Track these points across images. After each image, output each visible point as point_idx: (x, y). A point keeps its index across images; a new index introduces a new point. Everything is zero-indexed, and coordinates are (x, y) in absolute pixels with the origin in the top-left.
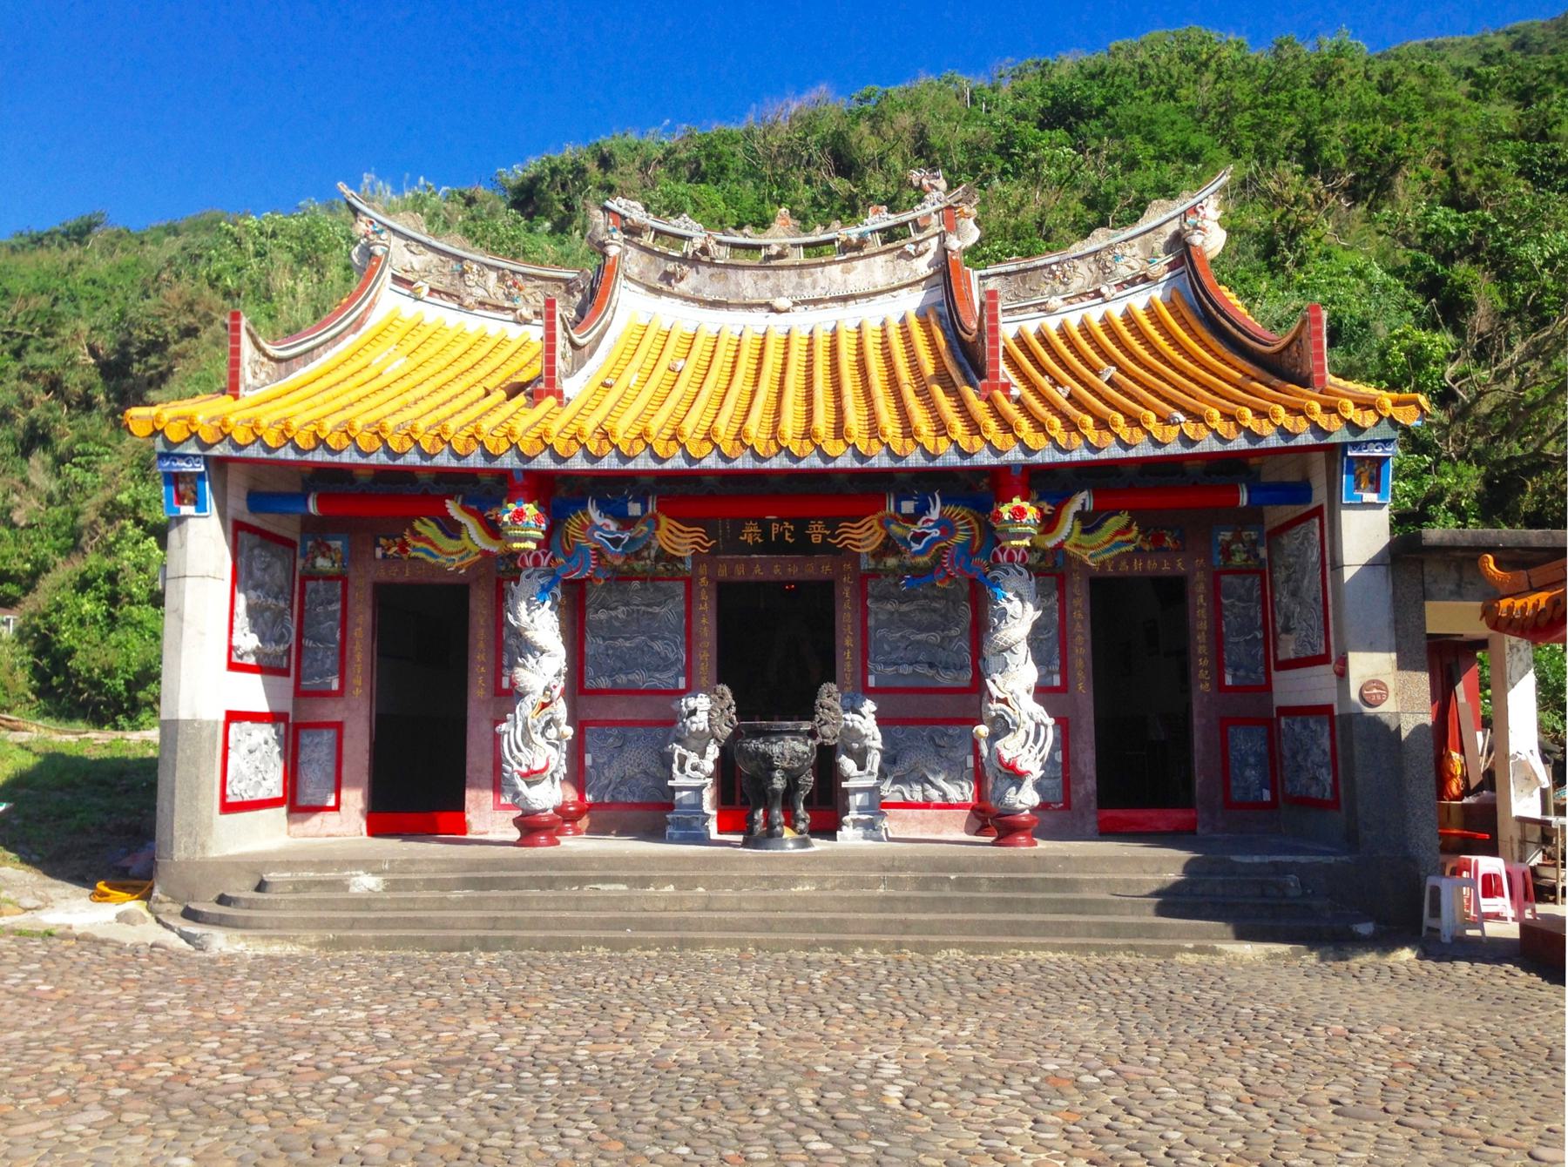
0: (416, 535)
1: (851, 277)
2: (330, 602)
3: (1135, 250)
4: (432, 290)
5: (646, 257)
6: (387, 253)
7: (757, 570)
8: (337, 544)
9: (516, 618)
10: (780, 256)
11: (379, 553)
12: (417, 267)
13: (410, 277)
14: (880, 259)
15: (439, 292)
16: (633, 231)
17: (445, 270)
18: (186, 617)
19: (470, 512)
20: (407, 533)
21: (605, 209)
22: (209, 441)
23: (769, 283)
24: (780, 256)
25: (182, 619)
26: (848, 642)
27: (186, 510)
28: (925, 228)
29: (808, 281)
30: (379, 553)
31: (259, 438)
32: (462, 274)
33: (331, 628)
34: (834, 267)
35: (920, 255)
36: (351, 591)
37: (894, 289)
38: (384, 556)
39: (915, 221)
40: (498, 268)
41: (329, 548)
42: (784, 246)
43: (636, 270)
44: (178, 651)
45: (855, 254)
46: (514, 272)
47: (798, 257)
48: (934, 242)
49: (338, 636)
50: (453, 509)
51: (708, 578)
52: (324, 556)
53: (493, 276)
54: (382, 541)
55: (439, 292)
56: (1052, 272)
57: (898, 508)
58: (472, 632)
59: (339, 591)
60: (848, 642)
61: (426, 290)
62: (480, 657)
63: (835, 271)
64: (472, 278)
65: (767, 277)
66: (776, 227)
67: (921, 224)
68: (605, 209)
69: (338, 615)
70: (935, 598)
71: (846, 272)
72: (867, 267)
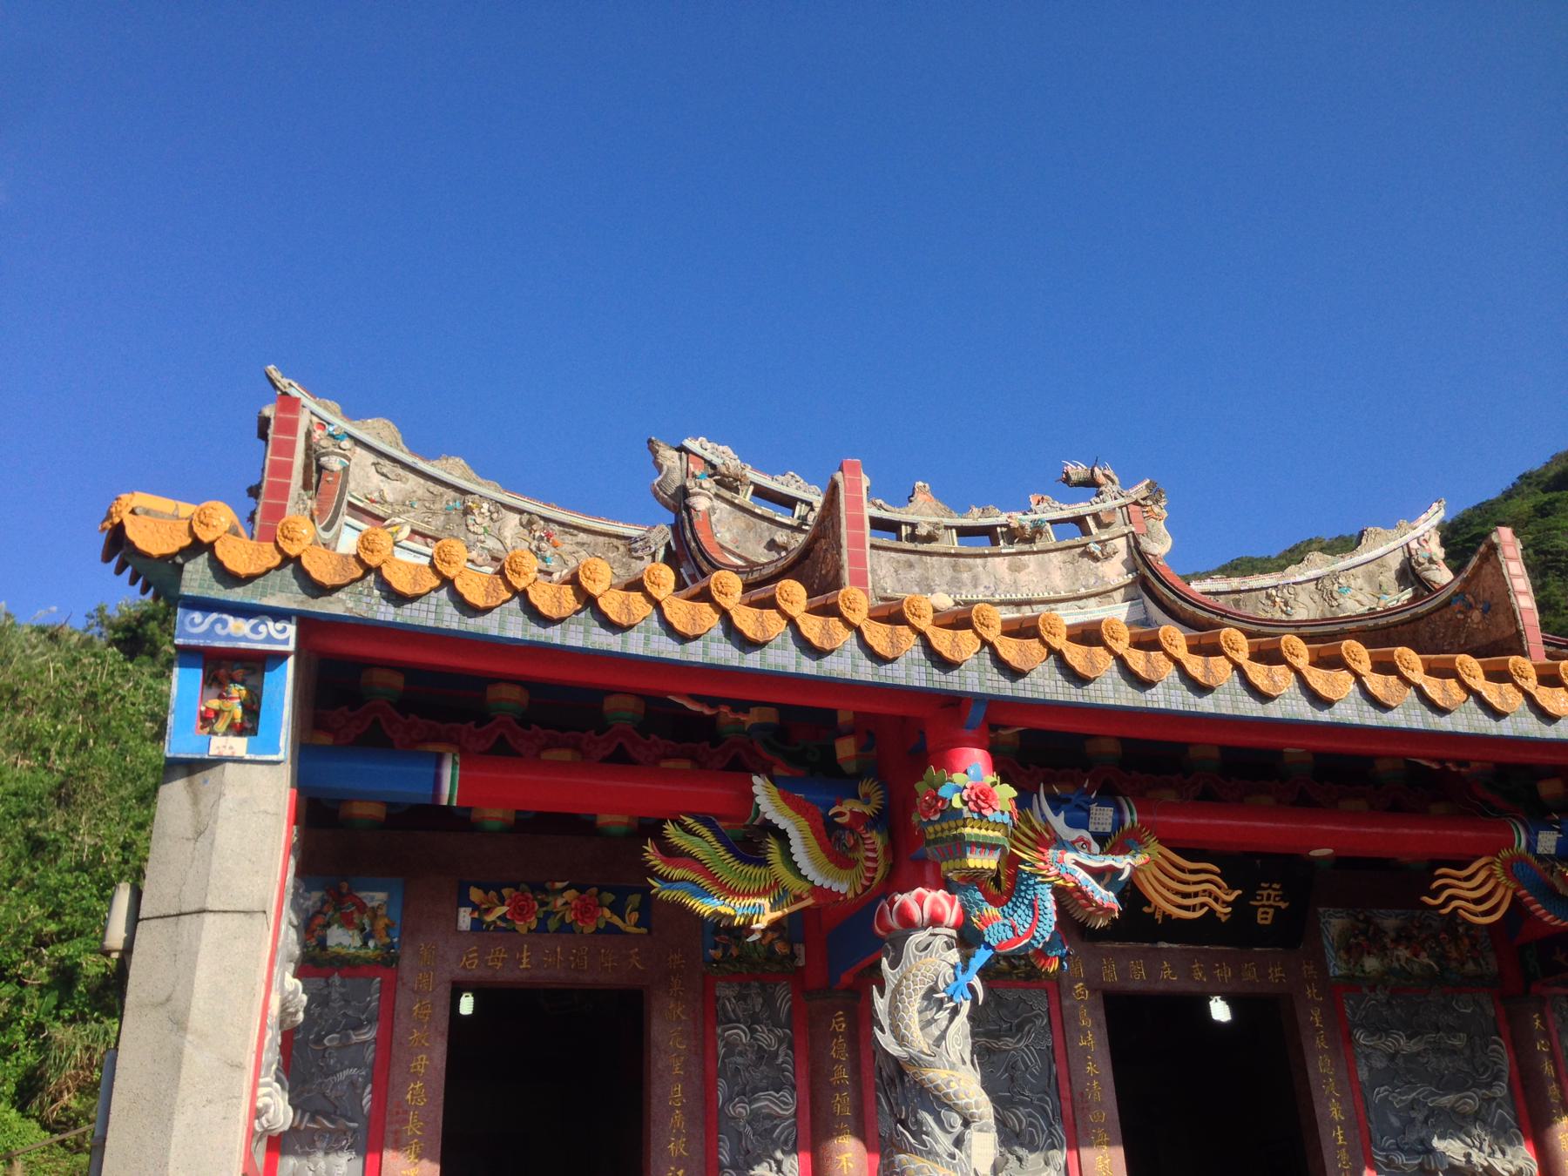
0: (671, 853)
1: (1023, 577)
2: (358, 1026)
3: (1360, 582)
4: (414, 532)
5: (744, 519)
6: (346, 469)
7: (1167, 973)
8: (375, 898)
9: (901, 1040)
10: (930, 538)
11: (465, 918)
12: (389, 497)
13: (378, 510)
14: (1056, 558)
15: (424, 536)
16: (727, 483)
17: (437, 506)
18: (196, 1018)
19: (798, 808)
20: (650, 848)
21: (681, 449)
22: (328, 580)
23: (914, 574)
24: (930, 538)
25: (180, 1024)
26: (1336, 1113)
27: (223, 744)
28: (1108, 525)
29: (966, 576)
30: (465, 918)
31: (447, 582)
32: (467, 511)
33: (352, 1083)
34: (997, 560)
35: (1107, 557)
36: (402, 1002)
37: (1080, 598)
38: (477, 924)
39: (1096, 516)
40: (521, 512)
41: (362, 907)
42: (936, 525)
43: (728, 536)
44: (162, 1113)
45: (1026, 547)
46: (547, 520)
47: (950, 542)
48: (1121, 544)
49: (367, 1100)
50: (767, 800)
51: (1088, 985)
52: (347, 922)
53: (514, 519)
54: (475, 894)
55: (424, 536)
56: (1269, 597)
57: (1531, 846)
58: (656, 1089)
59: (374, 1000)
60: (1336, 1113)
61: (406, 531)
62: (675, 1147)
63: (1000, 565)
64: (479, 521)
65: (911, 565)
66: (919, 498)
67: (1105, 520)
68: (681, 449)
69: (369, 1055)
70: (1452, 1030)
71: (1015, 569)
72: (1042, 567)
